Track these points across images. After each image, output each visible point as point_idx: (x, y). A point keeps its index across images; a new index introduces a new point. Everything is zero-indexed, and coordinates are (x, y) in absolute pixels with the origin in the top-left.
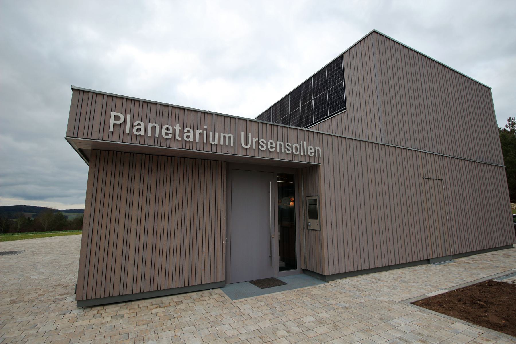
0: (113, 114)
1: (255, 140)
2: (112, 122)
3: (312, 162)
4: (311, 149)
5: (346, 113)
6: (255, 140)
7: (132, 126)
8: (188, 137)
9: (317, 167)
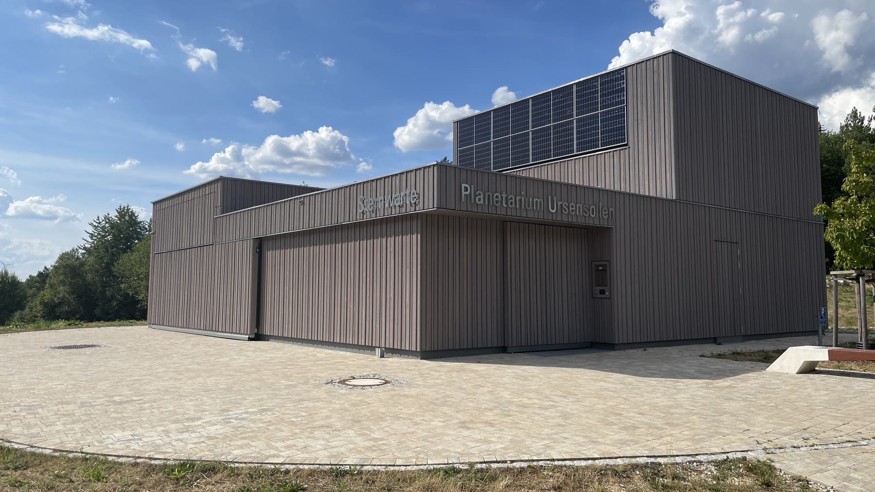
0: (463, 185)
1: (559, 203)
2: (464, 193)
3: (604, 224)
4: (497, 197)
5: (627, 151)
6: (559, 203)
7: (476, 196)
8: (511, 203)
9: (609, 229)
